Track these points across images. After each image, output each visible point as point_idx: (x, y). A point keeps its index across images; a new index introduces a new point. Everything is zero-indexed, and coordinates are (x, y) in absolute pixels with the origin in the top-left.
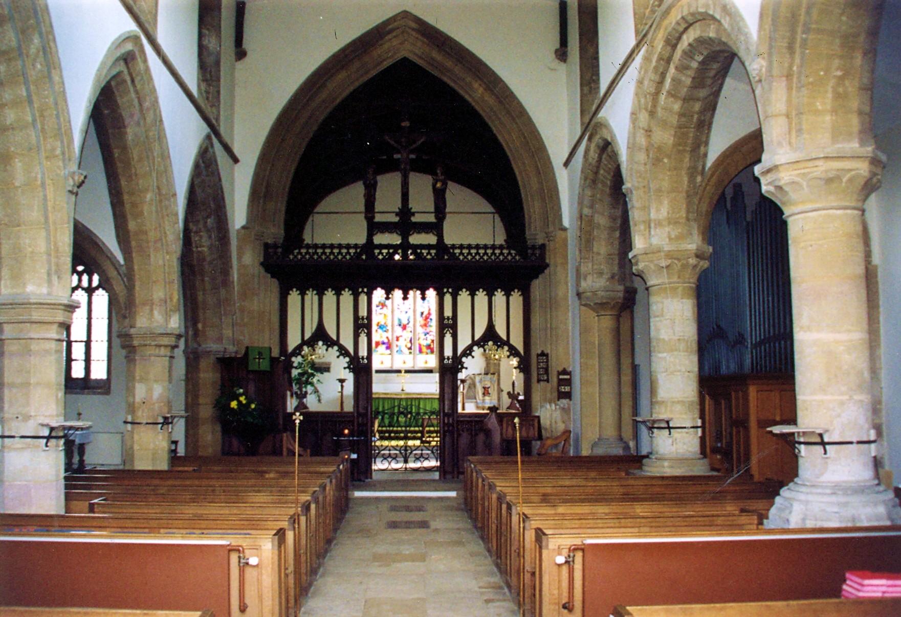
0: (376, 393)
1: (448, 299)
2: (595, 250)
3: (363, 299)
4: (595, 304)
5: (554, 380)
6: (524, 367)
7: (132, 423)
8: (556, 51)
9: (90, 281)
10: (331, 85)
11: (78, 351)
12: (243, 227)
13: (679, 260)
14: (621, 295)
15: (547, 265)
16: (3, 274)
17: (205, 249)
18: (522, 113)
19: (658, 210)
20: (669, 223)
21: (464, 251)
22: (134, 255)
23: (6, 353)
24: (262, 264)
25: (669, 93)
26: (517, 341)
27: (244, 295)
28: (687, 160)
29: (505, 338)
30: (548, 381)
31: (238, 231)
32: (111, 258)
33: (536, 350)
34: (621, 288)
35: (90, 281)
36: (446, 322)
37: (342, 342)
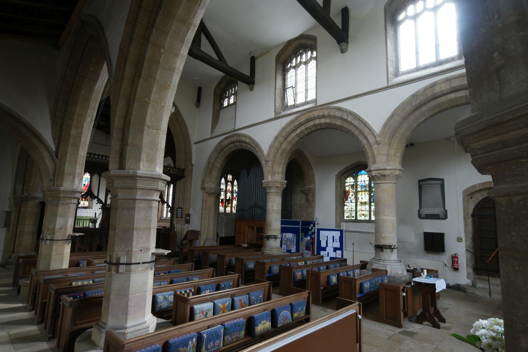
2: (213, 174)
6: (172, 210)
7: (50, 240)
15: (185, 177)
16: (142, 157)
18: (183, 121)
19: (279, 169)
22: (69, 148)
23: (136, 208)
25: (297, 135)
30: (181, 217)
33: (176, 206)
37: (99, 197)
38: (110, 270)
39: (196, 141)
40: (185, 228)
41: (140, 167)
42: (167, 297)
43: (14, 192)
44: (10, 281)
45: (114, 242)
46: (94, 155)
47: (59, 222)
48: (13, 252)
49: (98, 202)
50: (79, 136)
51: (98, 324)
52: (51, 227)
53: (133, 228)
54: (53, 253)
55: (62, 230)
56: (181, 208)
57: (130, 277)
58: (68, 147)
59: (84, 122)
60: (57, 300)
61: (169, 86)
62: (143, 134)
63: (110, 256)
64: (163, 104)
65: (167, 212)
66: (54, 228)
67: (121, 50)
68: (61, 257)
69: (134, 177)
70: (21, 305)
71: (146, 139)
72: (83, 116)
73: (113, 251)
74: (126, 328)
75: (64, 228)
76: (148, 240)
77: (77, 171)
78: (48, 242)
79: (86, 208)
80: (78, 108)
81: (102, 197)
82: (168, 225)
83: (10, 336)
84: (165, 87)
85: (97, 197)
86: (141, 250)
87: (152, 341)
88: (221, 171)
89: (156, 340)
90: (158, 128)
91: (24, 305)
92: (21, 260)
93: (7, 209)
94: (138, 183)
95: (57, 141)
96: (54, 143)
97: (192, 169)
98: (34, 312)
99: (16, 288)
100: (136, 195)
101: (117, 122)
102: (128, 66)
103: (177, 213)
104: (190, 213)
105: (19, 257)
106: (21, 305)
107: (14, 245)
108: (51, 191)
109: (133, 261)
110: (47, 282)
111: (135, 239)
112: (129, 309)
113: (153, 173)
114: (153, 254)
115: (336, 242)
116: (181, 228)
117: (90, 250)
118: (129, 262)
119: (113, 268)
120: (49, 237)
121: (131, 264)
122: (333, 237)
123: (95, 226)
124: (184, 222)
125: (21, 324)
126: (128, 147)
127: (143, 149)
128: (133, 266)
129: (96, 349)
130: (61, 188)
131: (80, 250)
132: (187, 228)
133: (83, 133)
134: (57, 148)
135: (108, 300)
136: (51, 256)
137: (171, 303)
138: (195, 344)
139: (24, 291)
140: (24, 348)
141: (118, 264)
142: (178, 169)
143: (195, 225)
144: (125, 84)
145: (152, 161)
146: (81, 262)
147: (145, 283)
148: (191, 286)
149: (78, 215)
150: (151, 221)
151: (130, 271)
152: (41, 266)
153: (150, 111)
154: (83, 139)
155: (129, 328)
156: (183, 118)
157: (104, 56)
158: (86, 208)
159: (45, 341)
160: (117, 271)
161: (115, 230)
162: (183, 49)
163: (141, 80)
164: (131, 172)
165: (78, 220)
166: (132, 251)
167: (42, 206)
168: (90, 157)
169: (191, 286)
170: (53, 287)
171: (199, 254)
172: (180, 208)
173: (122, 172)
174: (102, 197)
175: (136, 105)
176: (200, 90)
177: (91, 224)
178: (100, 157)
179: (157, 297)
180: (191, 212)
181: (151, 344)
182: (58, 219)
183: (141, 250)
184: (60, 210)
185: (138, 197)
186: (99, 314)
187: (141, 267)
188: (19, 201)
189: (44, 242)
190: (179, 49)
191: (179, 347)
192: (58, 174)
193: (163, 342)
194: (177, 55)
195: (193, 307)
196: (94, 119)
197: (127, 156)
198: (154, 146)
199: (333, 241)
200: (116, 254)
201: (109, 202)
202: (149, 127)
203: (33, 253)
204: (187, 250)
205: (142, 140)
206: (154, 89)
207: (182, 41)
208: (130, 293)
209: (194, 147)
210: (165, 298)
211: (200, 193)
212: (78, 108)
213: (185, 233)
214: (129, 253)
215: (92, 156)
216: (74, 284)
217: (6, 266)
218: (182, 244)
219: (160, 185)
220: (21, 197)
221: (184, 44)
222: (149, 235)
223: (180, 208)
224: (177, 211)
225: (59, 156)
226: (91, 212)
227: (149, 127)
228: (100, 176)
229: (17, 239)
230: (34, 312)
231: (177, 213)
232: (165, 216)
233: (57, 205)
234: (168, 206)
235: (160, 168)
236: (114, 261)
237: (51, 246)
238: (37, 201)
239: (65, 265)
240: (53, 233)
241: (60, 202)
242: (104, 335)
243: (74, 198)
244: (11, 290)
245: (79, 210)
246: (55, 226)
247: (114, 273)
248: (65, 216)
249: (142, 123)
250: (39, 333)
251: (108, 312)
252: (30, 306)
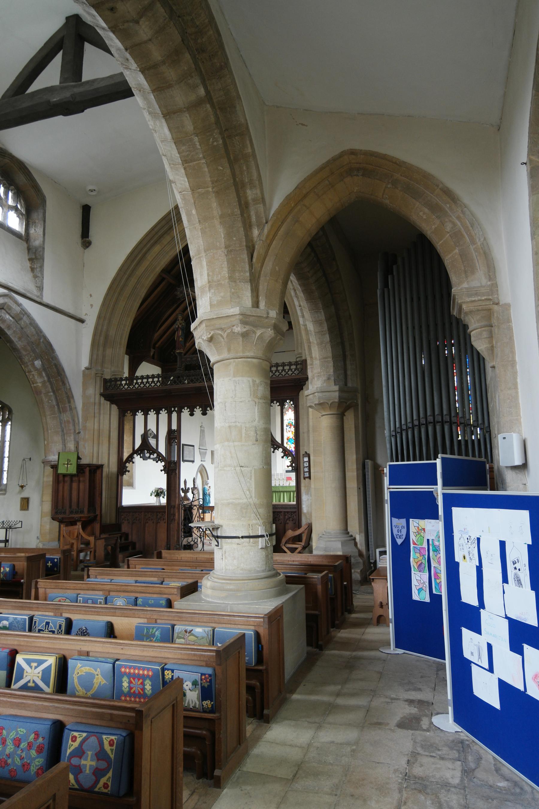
1: (174, 415)
3: (174, 415)
4: (315, 405)
6: (296, 467)
10: (150, 257)
12: (87, 369)
13: (222, 329)
14: (337, 394)
17: (40, 385)
20: (210, 287)
21: (285, 368)
24: (101, 395)
26: (291, 447)
27: (86, 419)
28: (214, 205)
29: (280, 442)
31: (84, 371)
33: (302, 452)
34: (336, 388)
85: (281, 445)
88: (327, 338)
115: (519, 582)
122: (502, 544)
174: (162, 449)
176: (86, 210)
199: (505, 580)
228: (158, 413)
244: (316, 593)
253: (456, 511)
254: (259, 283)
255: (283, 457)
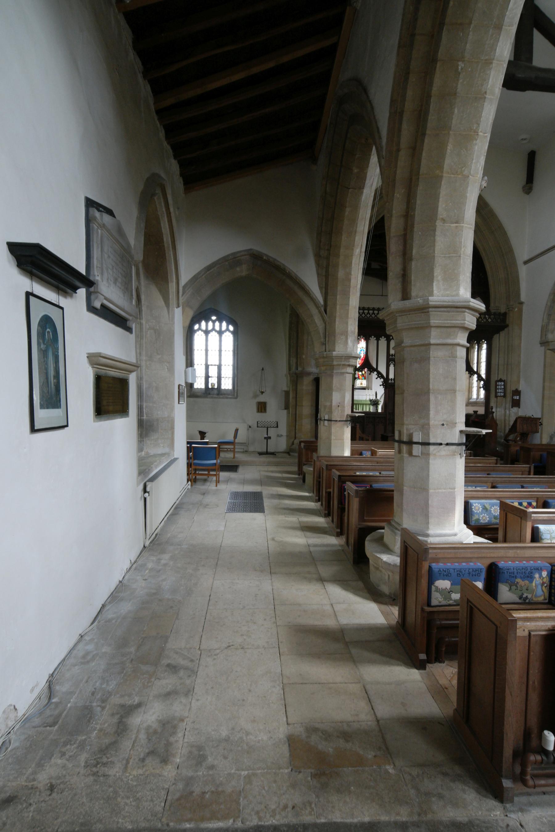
0: (357, 401)
5: (509, 395)
6: (487, 387)
7: (328, 420)
8: (523, 187)
9: (221, 326)
11: (213, 372)
15: (507, 326)
16: (435, 274)
18: (500, 227)
22: (338, 297)
23: (432, 359)
30: (504, 396)
32: (313, 300)
33: (494, 378)
35: (221, 326)
36: (391, 357)
37: (379, 369)
38: (400, 452)
39: (526, 258)
40: (512, 414)
41: (433, 291)
42: (488, 507)
43: (290, 369)
44: (295, 469)
45: (403, 410)
46: (369, 309)
47: (336, 397)
48: (295, 438)
49: (378, 377)
50: (348, 279)
51: (389, 522)
52: (328, 404)
53: (429, 389)
54: (333, 437)
55: (340, 408)
56: (504, 381)
57: (428, 463)
58: (336, 296)
59: (352, 256)
60: (342, 490)
61: (476, 132)
62: (434, 236)
63: (400, 432)
64: (466, 173)
65: (479, 388)
66: (331, 405)
67: (393, 102)
68: (341, 444)
69: (424, 309)
70: (307, 494)
71: (441, 243)
72: (351, 247)
73: (403, 424)
74: (428, 536)
75: (341, 405)
76: (453, 410)
77: (349, 329)
78: (326, 422)
79: (364, 389)
80: (344, 237)
81: (382, 369)
82: (481, 411)
83: (300, 522)
84: (468, 138)
85: (376, 370)
86: (443, 425)
87: (469, 555)
89: (476, 556)
90: (458, 220)
91: (311, 495)
92: (302, 445)
93: (285, 388)
94: (431, 318)
95: (324, 289)
96: (321, 292)
97: (521, 310)
98: (320, 503)
99: (301, 476)
100: (430, 337)
101: (393, 247)
102: (405, 126)
103: (496, 389)
104: (520, 389)
105: (300, 442)
106: (307, 494)
107: (295, 430)
108: (324, 357)
109: (432, 441)
110: (329, 467)
111: (432, 406)
112: (430, 509)
113: (455, 299)
114: (461, 432)
116: (505, 415)
117: (374, 439)
118: (427, 441)
119: (405, 448)
120: (326, 418)
121: (429, 444)
123: (377, 410)
124: (509, 404)
125: (309, 514)
126: (413, 263)
127: (436, 259)
128: (432, 448)
129: (391, 554)
130: (334, 353)
131: (361, 439)
132: (514, 413)
133: (352, 273)
134: (325, 300)
135: (401, 492)
136: (331, 440)
137: (495, 517)
138: (547, 580)
139: (309, 479)
140: (314, 538)
141: (410, 443)
142: (495, 314)
143: (530, 407)
144: (399, 194)
145: (451, 278)
146: (364, 452)
147: (452, 476)
148: (531, 497)
149: (356, 398)
150: (455, 379)
151: (428, 454)
152: (322, 452)
153: (444, 191)
154: (353, 281)
155: (433, 536)
156: (499, 221)
157: (370, 137)
158: (364, 389)
159: (334, 536)
160: (410, 454)
161: (402, 393)
162: (500, 44)
163: (426, 141)
164: (420, 301)
165: (356, 404)
166: (429, 424)
167: (317, 381)
168: (363, 313)
169: (531, 497)
170: (336, 473)
171: (541, 455)
172: (501, 380)
173: (407, 304)
174: (382, 369)
175: (420, 188)
176: (532, 157)
177: (371, 407)
178: (371, 312)
179: (472, 505)
180: (522, 387)
181: (468, 560)
182: (334, 393)
183: (443, 425)
184: (336, 381)
185: (432, 341)
186: (391, 512)
187: (444, 450)
188: (296, 377)
189: (322, 422)
190: (493, 48)
191: (516, 577)
192: (329, 336)
193: (488, 562)
194: (488, 63)
195: (538, 528)
196: (364, 249)
197: (413, 278)
198: (454, 251)
200: (407, 429)
201: (391, 376)
202: (443, 220)
203: (314, 440)
204: (518, 448)
205: (434, 246)
206: (450, 147)
207: (499, 27)
208: (430, 486)
209: (523, 271)
210: (485, 508)
211: (539, 351)
212: (343, 237)
213: (512, 423)
214: (425, 428)
215: (366, 312)
216: (358, 473)
217: (291, 453)
218: (507, 440)
219: (467, 319)
220: (296, 374)
221: (503, 33)
222: (453, 401)
223: (501, 380)
224: (496, 385)
225: (328, 310)
226: (370, 392)
227: (443, 220)
228: (378, 340)
229: (297, 423)
230: (320, 503)
231: (496, 389)
232: (474, 396)
233: (331, 376)
234: (480, 378)
235: (466, 289)
236: (405, 439)
237: (330, 427)
238: (311, 378)
239: (347, 453)
240: (330, 412)
241: (335, 371)
242: (398, 539)
243: (349, 366)
244: (297, 478)
245: (356, 392)
246: (332, 402)
247: (406, 455)
248: (341, 389)
249: (432, 216)
250: (326, 525)
251: (402, 509)
252: (316, 496)
253: (36, 428)
254: (412, 231)
255: (377, 378)
